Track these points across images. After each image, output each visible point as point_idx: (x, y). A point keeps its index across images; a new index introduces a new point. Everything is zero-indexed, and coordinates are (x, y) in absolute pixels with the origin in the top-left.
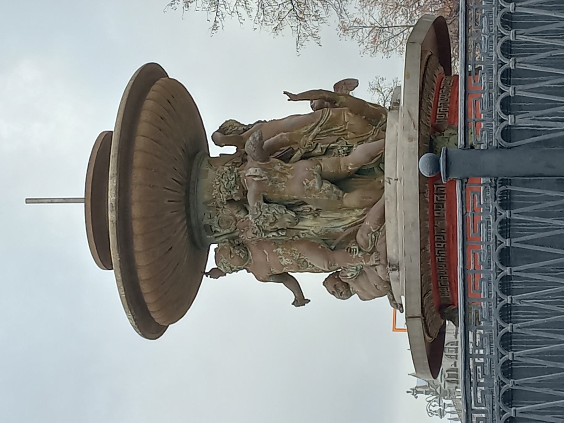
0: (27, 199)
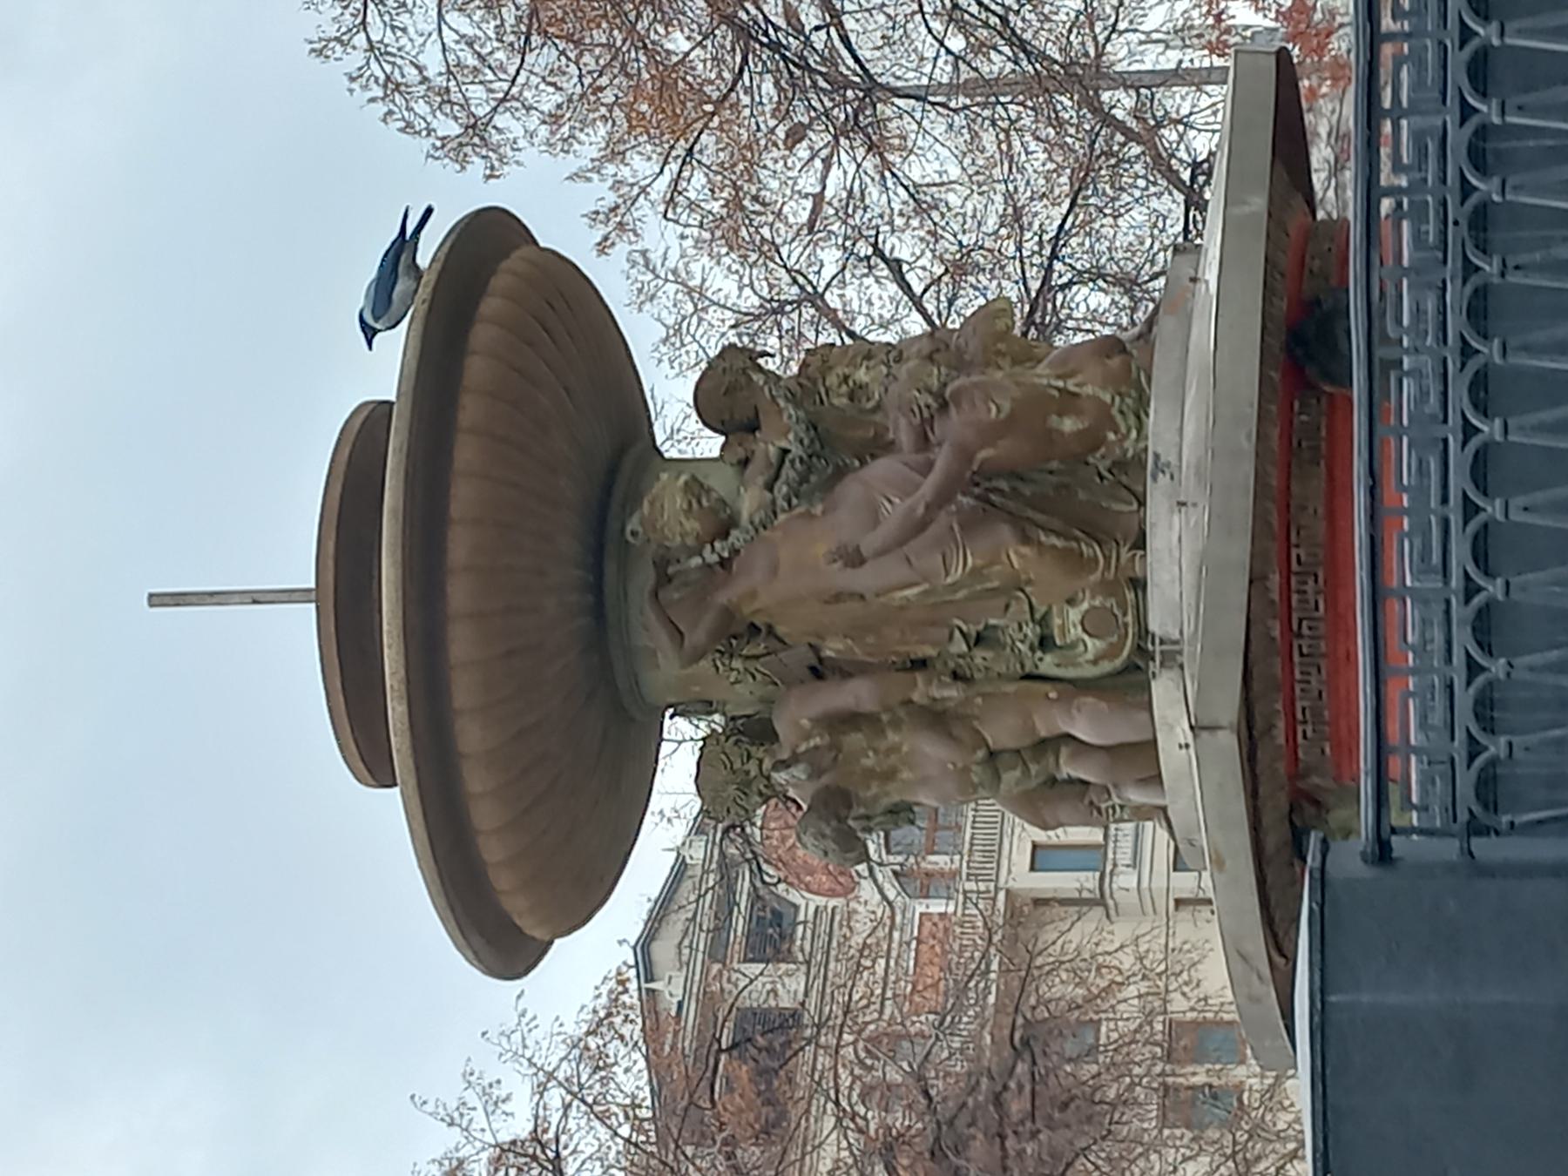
0: (151, 596)
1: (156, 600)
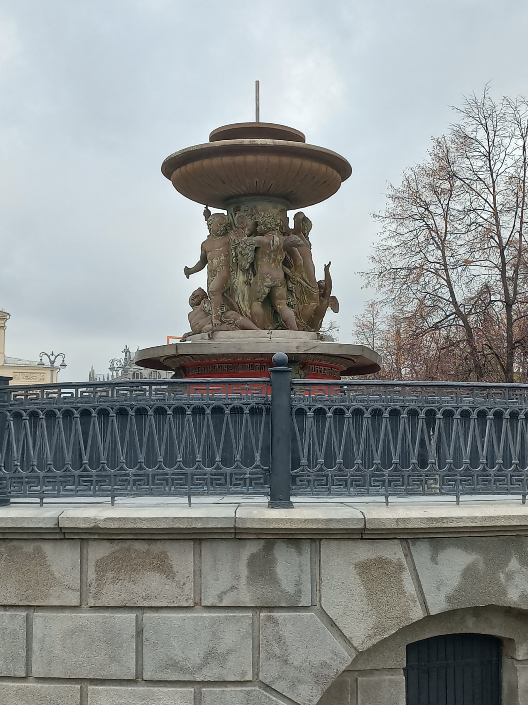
0: (258, 81)
1: (257, 83)
